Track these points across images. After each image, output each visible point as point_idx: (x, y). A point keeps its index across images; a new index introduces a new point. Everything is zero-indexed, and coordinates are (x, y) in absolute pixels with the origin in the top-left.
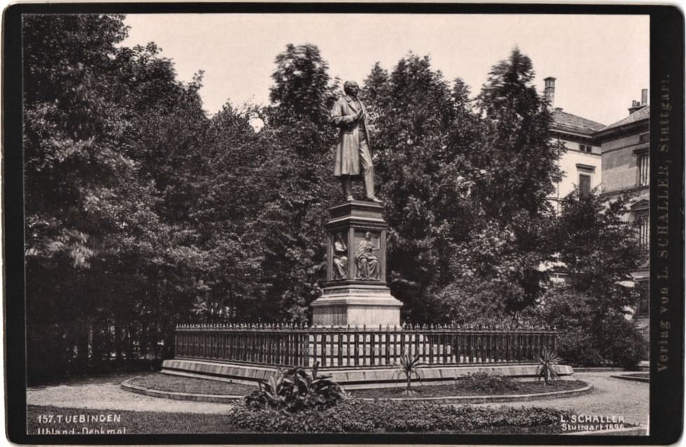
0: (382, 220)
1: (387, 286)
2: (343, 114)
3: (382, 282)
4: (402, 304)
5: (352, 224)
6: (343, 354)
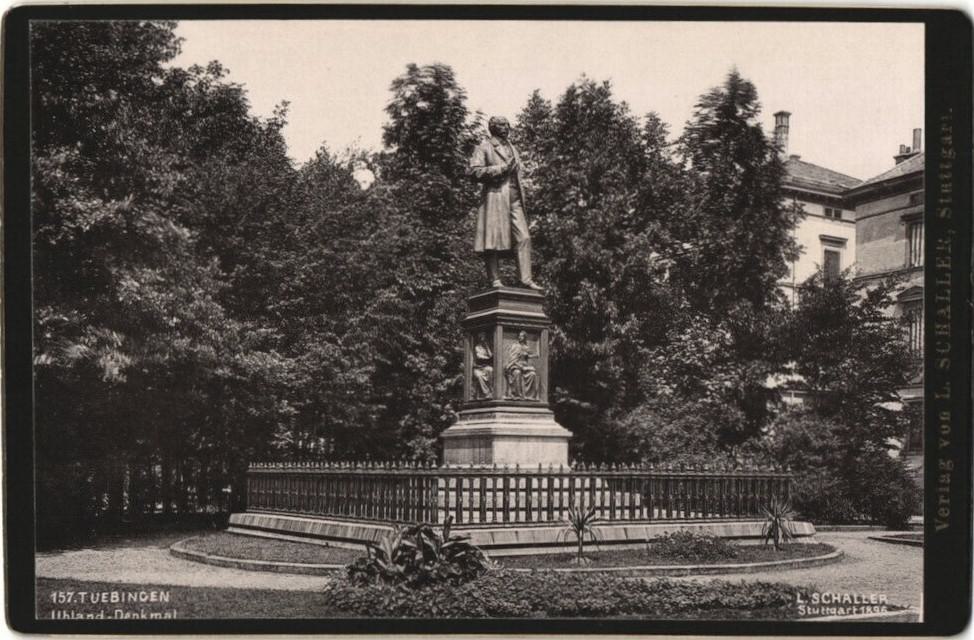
0: (543, 315)
1: (550, 408)
3: (542, 402)
4: (570, 434)
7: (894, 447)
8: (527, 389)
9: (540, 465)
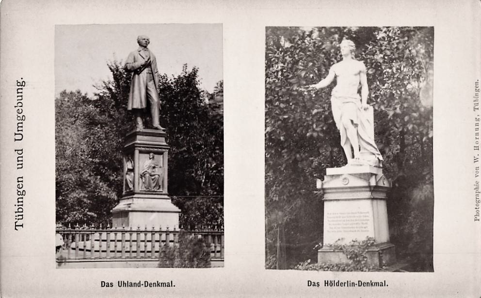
0: (165, 144)
1: (168, 195)
3: (164, 192)
4: (180, 210)
5: (137, 147)
7: (301, 66)
8: (154, 185)
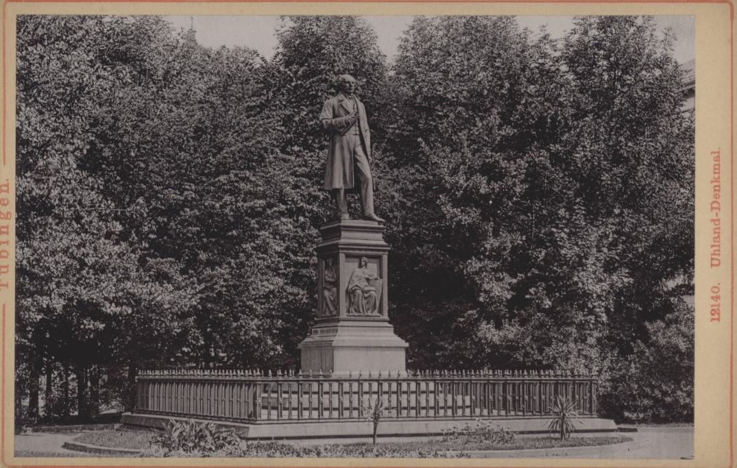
1: (390, 322)
2: (335, 116)
4: (407, 345)
6: (304, 406)
9: (390, 373)
